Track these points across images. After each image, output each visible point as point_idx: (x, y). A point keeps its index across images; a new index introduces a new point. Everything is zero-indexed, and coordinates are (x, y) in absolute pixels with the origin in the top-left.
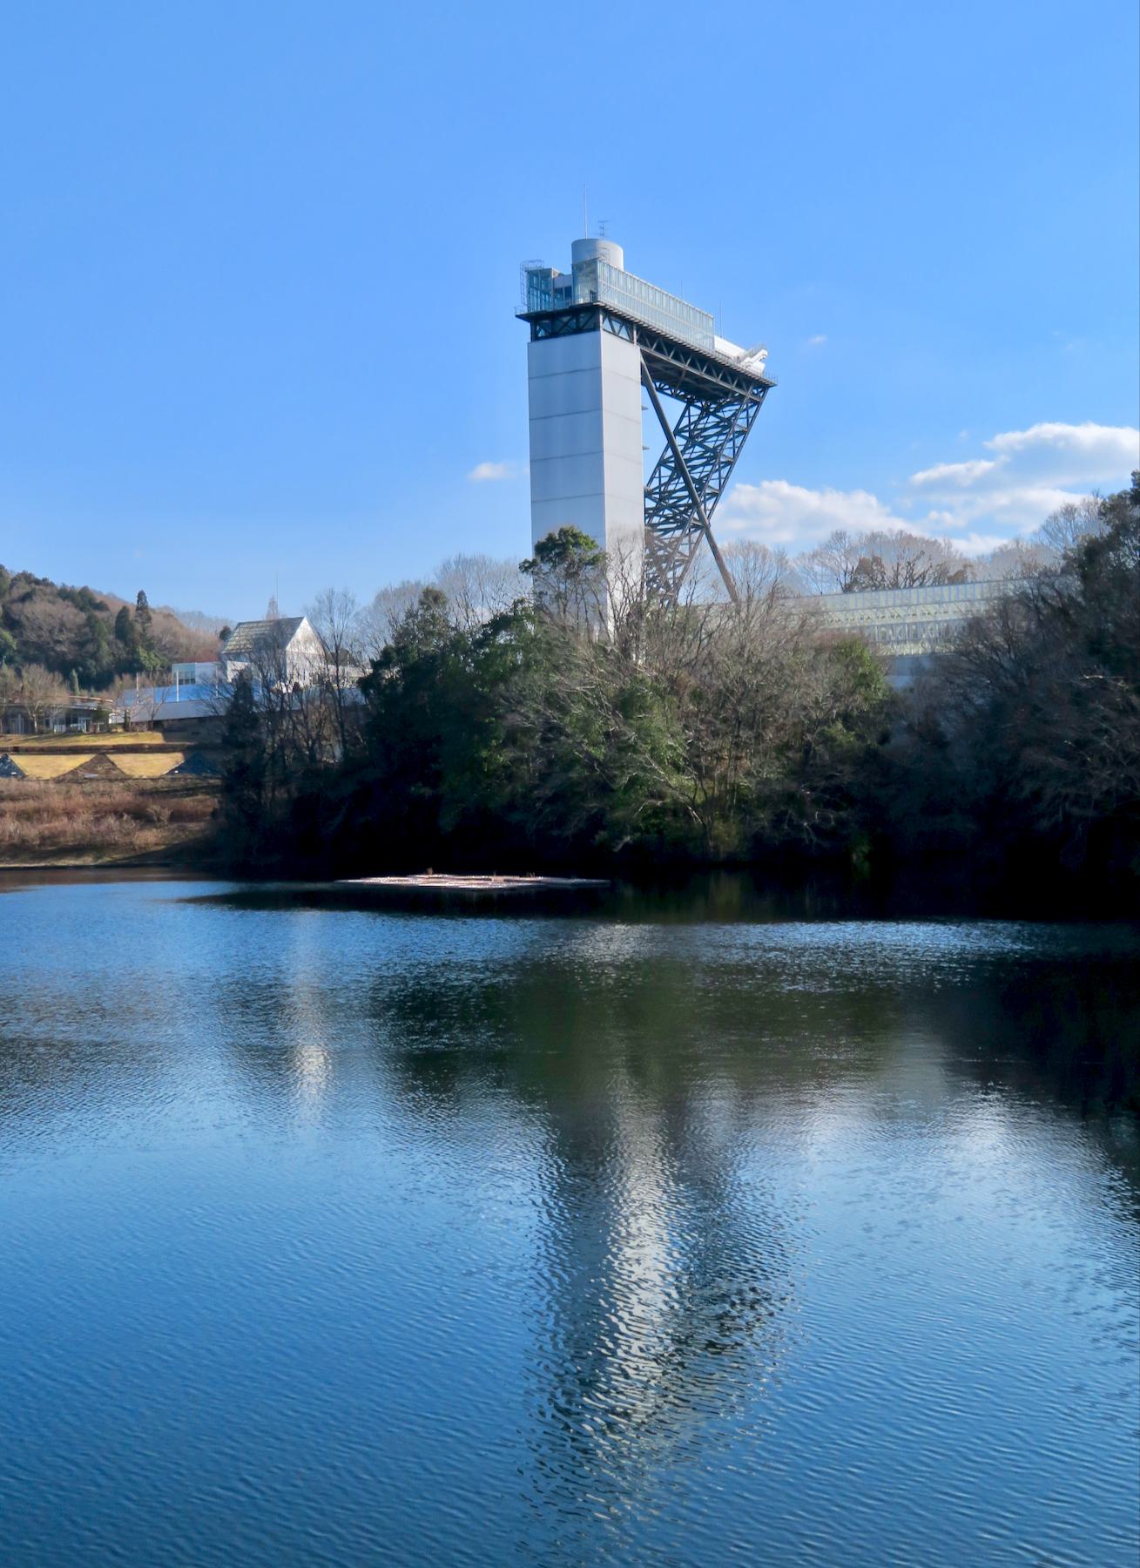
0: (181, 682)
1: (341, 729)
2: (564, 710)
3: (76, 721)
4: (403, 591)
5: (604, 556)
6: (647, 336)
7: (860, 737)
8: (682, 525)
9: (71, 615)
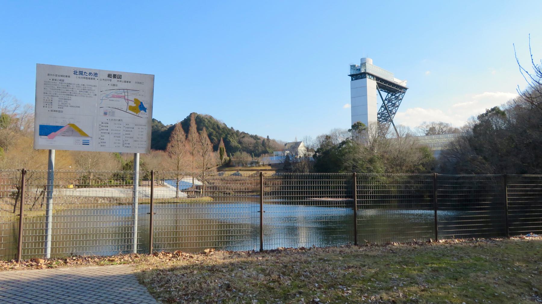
0: (275, 156)
1: (309, 167)
2: (357, 162)
3: (253, 164)
4: (322, 137)
5: (367, 128)
6: (378, 79)
7: (426, 169)
8: (386, 120)
9: (253, 141)
